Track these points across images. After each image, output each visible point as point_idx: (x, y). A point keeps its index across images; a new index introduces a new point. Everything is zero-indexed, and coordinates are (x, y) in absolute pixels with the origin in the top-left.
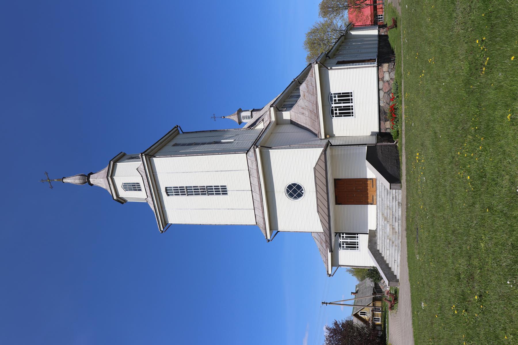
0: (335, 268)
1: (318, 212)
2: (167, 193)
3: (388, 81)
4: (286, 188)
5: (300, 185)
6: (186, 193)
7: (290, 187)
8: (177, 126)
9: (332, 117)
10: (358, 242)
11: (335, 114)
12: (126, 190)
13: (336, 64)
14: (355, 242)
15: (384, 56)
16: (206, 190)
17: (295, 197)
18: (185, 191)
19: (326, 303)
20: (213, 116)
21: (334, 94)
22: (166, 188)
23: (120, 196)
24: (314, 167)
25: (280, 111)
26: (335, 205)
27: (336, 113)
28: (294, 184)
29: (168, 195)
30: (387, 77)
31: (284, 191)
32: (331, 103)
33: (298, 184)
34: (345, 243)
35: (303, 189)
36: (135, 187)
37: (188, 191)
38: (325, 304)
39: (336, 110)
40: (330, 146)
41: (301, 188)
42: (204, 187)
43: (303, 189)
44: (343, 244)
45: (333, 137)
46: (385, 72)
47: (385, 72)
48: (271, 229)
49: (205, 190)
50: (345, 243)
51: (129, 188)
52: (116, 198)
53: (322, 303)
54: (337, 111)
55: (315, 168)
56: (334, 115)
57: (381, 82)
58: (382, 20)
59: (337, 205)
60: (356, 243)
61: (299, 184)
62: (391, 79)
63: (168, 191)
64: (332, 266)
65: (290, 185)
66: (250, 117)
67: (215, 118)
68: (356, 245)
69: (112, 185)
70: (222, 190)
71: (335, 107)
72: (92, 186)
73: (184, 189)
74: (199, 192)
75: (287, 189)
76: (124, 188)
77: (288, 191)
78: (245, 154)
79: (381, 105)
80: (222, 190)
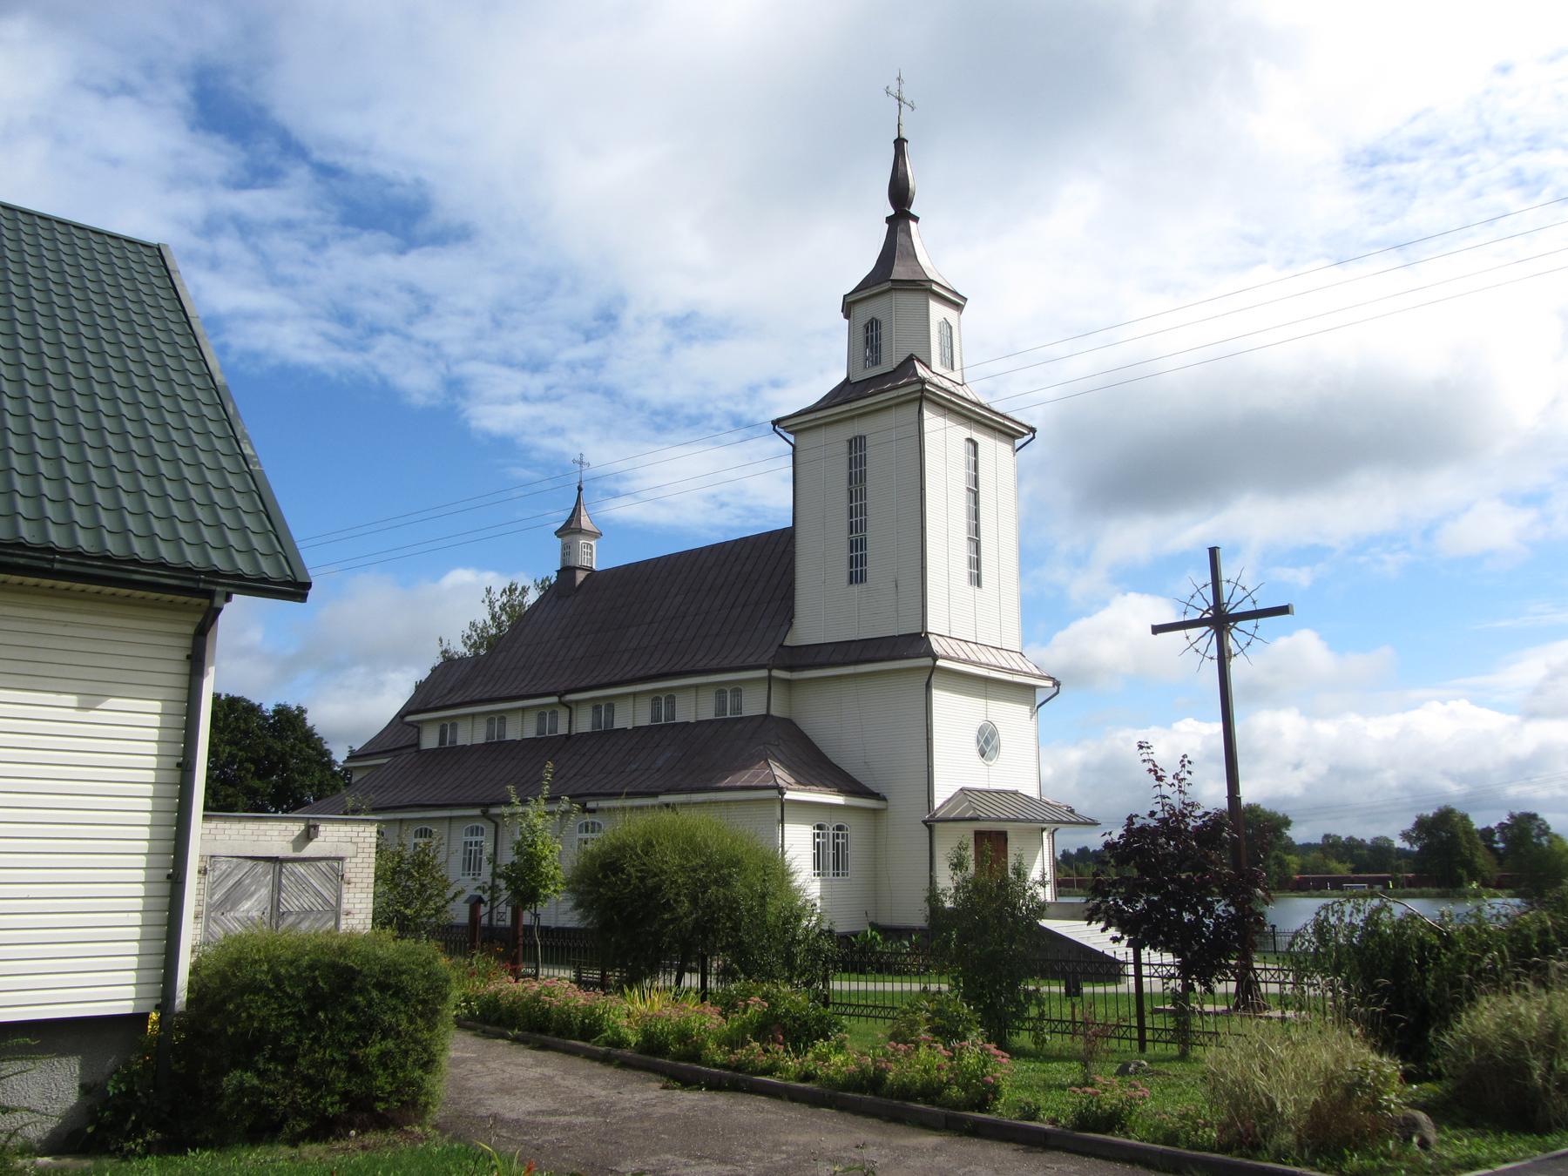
52: (850, 300)
60: (477, 872)
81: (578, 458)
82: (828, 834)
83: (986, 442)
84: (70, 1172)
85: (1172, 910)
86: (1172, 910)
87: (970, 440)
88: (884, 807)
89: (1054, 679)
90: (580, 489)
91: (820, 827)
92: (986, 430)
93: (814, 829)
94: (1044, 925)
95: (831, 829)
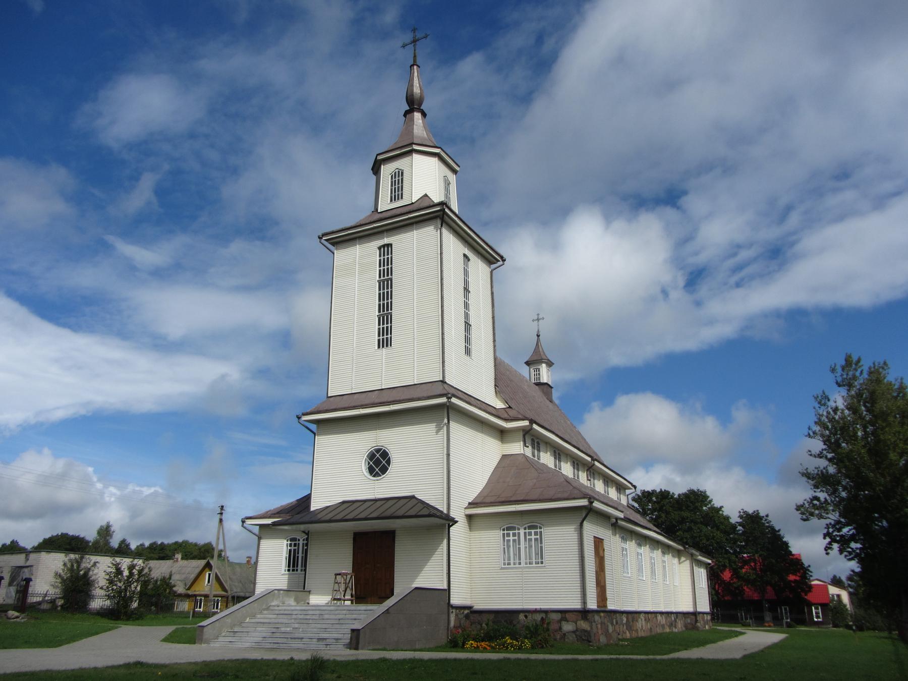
0: (256, 530)
1: (344, 502)
2: (384, 246)
3: (560, 628)
4: (384, 448)
5: (388, 471)
6: (382, 278)
7: (385, 454)
8: (505, 260)
9: (525, 526)
10: (297, 570)
11: (507, 533)
12: (392, 177)
13: (594, 537)
14: (297, 567)
15: (615, 623)
16: (386, 312)
17: (369, 463)
18: (386, 277)
19: (221, 514)
20: (541, 317)
21: (541, 532)
22: (391, 245)
23: (382, 166)
24: (416, 496)
25: (524, 436)
26: (352, 532)
27: (508, 535)
28: (389, 462)
29: (380, 248)
30: (567, 627)
31: (379, 445)
32: (525, 526)
33: (389, 468)
34: (296, 548)
35: (381, 477)
36: (397, 192)
37: (386, 282)
38: (219, 512)
39: (514, 535)
40: (449, 524)
41: (383, 474)
42: (391, 310)
43: (381, 476)
44: (295, 545)
45: (470, 529)
46: (576, 624)
47: (576, 624)
48: (318, 422)
49: (387, 311)
50: (296, 548)
51: (395, 181)
52: (380, 158)
53: (222, 507)
54: (535, 535)
55: (413, 497)
56: (527, 531)
57: (558, 616)
58: (742, 620)
59: (353, 535)
60: (295, 568)
61: (389, 470)
62: (564, 634)
63: (382, 249)
64: (261, 526)
65: (388, 454)
66: (538, 381)
67: (538, 320)
68: (293, 567)
69: (399, 152)
70: (385, 341)
71: (519, 534)
72: (404, 115)
73: (388, 275)
74: (383, 301)
75: (382, 449)
76: (395, 173)
77: (378, 451)
78: (441, 379)
79: (520, 616)
80: (385, 341)
81: (541, 317)
82: (299, 544)
83: (474, 259)
84: (806, 597)
85: (767, 530)
86: (767, 530)
87: (465, 255)
88: (466, 510)
89: (299, 422)
90: (538, 336)
91: (291, 540)
92: (372, 238)
93: (287, 541)
94: (169, 627)
95: (301, 540)
